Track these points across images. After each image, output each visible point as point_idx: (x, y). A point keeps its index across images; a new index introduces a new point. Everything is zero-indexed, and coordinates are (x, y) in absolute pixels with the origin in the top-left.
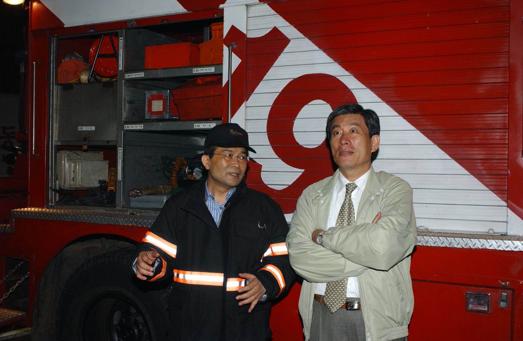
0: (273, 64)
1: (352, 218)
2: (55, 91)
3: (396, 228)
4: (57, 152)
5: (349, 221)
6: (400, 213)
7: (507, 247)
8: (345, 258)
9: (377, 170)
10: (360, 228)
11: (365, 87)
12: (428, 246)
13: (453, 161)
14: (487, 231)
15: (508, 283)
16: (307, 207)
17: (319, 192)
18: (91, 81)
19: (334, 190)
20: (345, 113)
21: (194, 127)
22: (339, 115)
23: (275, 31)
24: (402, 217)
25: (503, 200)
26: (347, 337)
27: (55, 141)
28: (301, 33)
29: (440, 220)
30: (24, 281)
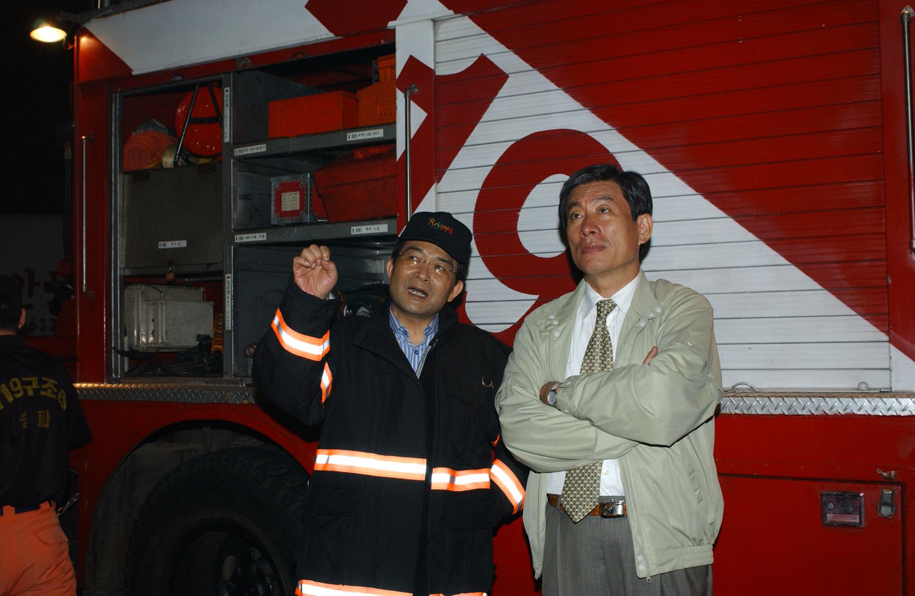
0: (481, 117)
1: (608, 359)
2: (119, 184)
3: (683, 371)
4: (124, 289)
5: (603, 366)
6: (690, 346)
7: (889, 410)
8: (594, 426)
9: (652, 277)
10: (620, 373)
11: (636, 148)
12: (751, 415)
13: (793, 267)
14: (856, 386)
15: (893, 472)
16: (531, 344)
17: (552, 318)
18: (179, 164)
19: (576, 313)
20: (589, 180)
21: (350, 232)
22: (577, 185)
23: (483, 62)
24: (694, 352)
25: (882, 331)
26: (605, 566)
27: (120, 269)
28: (527, 62)
29: (775, 372)
30: (70, 507)
